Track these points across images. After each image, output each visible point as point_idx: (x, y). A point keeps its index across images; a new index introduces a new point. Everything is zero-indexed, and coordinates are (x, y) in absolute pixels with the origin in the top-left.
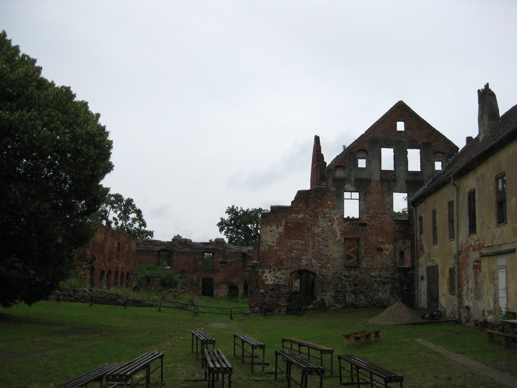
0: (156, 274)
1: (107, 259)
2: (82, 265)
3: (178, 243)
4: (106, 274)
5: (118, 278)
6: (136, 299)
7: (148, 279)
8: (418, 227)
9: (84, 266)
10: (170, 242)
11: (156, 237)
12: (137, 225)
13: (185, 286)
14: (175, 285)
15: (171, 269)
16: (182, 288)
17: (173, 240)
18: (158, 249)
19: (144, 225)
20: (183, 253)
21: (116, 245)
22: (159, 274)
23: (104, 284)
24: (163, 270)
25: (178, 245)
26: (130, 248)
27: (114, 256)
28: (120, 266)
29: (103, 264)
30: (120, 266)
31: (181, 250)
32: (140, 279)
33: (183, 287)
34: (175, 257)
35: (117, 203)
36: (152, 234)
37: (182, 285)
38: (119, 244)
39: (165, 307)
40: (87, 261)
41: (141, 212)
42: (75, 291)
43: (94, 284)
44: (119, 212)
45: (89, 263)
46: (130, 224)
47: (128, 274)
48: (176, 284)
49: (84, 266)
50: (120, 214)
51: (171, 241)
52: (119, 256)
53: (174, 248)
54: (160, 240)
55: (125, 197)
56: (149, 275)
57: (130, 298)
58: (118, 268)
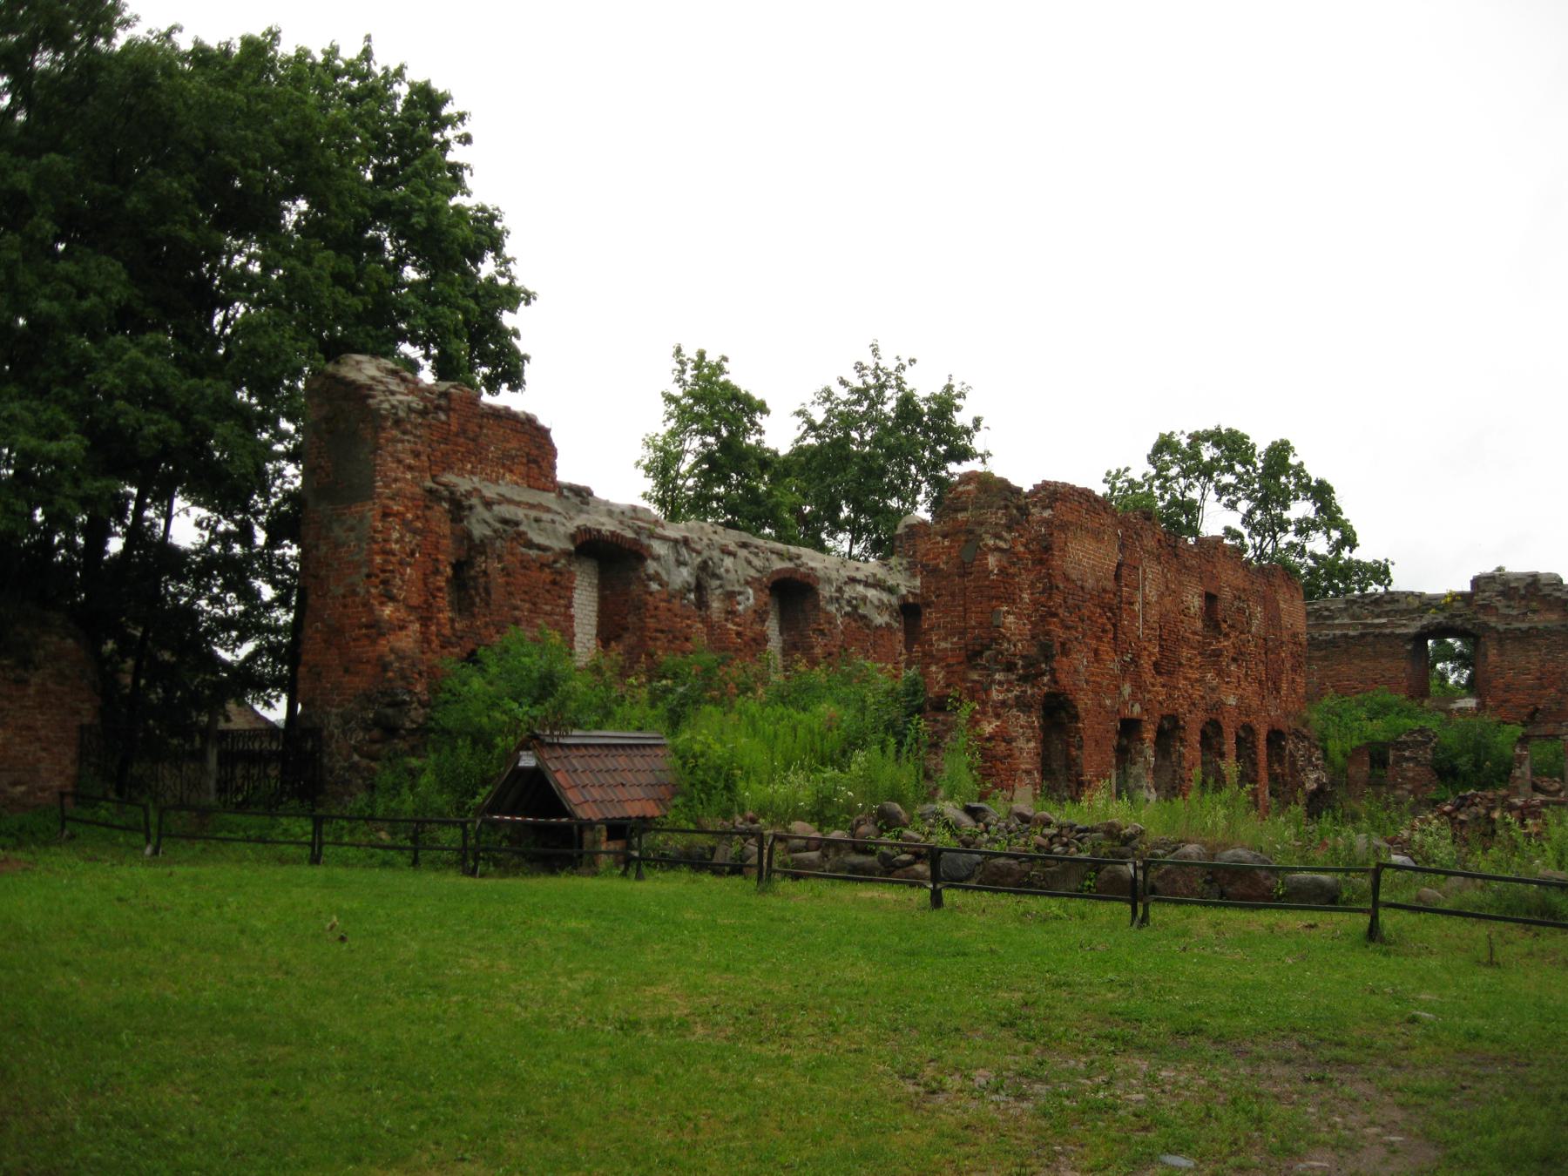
0: (1412, 732)
1: (1146, 664)
2: (987, 691)
3: (1502, 594)
4: (1149, 735)
5: (1222, 755)
6: (1226, 856)
7: (1378, 756)
8: (1314, 875)
9: (996, 695)
10: (1463, 595)
11: (1402, 581)
12: (1319, 544)
13: (1550, 775)
14: (1504, 773)
15: (1482, 707)
16: (1536, 788)
17: (1476, 582)
18: (1413, 628)
19: (1349, 540)
20: (1526, 637)
21: (1195, 603)
22: (1422, 731)
23: (1147, 780)
24: (1443, 716)
25: (1500, 603)
26: (1273, 619)
27: (1185, 653)
28: (1232, 701)
29: (1127, 689)
30: (1232, 701)
31: (1516, 625)
32: (1339, 759)
33: (1545, 782)
34: (1492, 653)
35: (1230, 469)
36: (1386, 572)
37: (1534, 773)
38: (1210, 599)
39: (1419, 908)
40: (1010, 667)
41: (1329, 490)
42: (887, 821)
43: (1081, 784)
44: (1244, 506)
45: (1023, 679)
46: (1291, 546)
47: (1275, 737)
48: (1508, 772)
49: (996, 695)
50: (1250, 513)
51: (1467, 588)
52: (1218, 654)
53: (1483, 618)
54: (1417, 590)
55: (1261, 443)
56: (1380, 737)
57: (1191, 849)
58: (1219, 706)
